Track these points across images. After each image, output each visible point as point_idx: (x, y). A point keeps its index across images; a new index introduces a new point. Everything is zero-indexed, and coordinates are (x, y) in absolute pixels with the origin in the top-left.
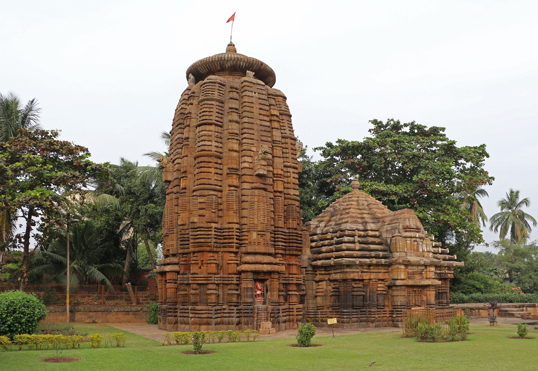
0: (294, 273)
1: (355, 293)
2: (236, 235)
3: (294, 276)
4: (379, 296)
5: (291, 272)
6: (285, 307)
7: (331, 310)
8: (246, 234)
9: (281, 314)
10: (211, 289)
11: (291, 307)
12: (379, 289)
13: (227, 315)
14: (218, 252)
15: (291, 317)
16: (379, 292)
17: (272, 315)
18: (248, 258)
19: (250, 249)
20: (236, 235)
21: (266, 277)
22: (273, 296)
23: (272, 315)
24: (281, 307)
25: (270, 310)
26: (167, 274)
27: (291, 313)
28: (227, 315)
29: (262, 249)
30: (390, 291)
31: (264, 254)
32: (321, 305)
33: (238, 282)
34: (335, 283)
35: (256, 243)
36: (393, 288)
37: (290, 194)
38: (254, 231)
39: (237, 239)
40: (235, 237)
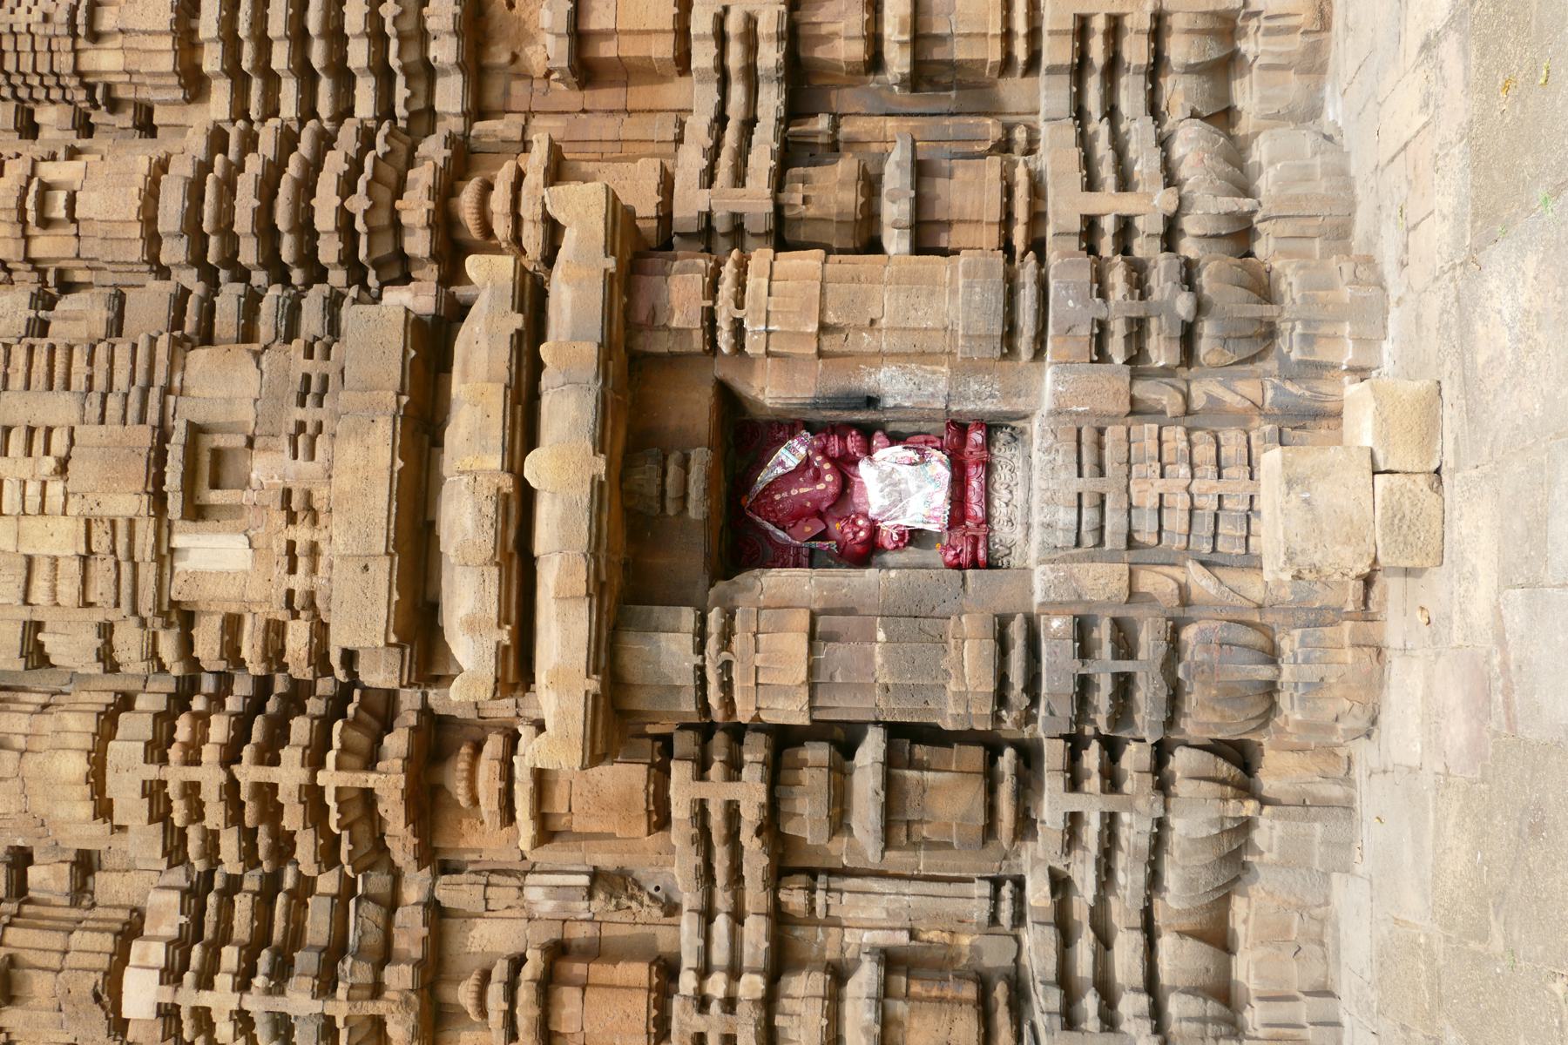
2: (230, 756)
5: (663, 48)
6: (1056, 155)
8: (207, 644)
9: (1149, 204)
11: (1057, 52)
13: (1129, 877)
14: (436, 913)
15: (1178, 50)
17: (1161, 352)
18: (471, 645)
19: (363, 620)
20: (230, 756)
21: (694, 409)
22: (911, 322)
23: (1161, 352)
24: (1066, 206)
25: (1108, 386)
26: (920, 157)
27: (1135, 51)
28: (1129, 877)
29: (363, 462)
31: (423, 425)
33: (754, 753)
35: (302, 534)
38: (165, 556)
39: (269, 755)
40: (248, 773)
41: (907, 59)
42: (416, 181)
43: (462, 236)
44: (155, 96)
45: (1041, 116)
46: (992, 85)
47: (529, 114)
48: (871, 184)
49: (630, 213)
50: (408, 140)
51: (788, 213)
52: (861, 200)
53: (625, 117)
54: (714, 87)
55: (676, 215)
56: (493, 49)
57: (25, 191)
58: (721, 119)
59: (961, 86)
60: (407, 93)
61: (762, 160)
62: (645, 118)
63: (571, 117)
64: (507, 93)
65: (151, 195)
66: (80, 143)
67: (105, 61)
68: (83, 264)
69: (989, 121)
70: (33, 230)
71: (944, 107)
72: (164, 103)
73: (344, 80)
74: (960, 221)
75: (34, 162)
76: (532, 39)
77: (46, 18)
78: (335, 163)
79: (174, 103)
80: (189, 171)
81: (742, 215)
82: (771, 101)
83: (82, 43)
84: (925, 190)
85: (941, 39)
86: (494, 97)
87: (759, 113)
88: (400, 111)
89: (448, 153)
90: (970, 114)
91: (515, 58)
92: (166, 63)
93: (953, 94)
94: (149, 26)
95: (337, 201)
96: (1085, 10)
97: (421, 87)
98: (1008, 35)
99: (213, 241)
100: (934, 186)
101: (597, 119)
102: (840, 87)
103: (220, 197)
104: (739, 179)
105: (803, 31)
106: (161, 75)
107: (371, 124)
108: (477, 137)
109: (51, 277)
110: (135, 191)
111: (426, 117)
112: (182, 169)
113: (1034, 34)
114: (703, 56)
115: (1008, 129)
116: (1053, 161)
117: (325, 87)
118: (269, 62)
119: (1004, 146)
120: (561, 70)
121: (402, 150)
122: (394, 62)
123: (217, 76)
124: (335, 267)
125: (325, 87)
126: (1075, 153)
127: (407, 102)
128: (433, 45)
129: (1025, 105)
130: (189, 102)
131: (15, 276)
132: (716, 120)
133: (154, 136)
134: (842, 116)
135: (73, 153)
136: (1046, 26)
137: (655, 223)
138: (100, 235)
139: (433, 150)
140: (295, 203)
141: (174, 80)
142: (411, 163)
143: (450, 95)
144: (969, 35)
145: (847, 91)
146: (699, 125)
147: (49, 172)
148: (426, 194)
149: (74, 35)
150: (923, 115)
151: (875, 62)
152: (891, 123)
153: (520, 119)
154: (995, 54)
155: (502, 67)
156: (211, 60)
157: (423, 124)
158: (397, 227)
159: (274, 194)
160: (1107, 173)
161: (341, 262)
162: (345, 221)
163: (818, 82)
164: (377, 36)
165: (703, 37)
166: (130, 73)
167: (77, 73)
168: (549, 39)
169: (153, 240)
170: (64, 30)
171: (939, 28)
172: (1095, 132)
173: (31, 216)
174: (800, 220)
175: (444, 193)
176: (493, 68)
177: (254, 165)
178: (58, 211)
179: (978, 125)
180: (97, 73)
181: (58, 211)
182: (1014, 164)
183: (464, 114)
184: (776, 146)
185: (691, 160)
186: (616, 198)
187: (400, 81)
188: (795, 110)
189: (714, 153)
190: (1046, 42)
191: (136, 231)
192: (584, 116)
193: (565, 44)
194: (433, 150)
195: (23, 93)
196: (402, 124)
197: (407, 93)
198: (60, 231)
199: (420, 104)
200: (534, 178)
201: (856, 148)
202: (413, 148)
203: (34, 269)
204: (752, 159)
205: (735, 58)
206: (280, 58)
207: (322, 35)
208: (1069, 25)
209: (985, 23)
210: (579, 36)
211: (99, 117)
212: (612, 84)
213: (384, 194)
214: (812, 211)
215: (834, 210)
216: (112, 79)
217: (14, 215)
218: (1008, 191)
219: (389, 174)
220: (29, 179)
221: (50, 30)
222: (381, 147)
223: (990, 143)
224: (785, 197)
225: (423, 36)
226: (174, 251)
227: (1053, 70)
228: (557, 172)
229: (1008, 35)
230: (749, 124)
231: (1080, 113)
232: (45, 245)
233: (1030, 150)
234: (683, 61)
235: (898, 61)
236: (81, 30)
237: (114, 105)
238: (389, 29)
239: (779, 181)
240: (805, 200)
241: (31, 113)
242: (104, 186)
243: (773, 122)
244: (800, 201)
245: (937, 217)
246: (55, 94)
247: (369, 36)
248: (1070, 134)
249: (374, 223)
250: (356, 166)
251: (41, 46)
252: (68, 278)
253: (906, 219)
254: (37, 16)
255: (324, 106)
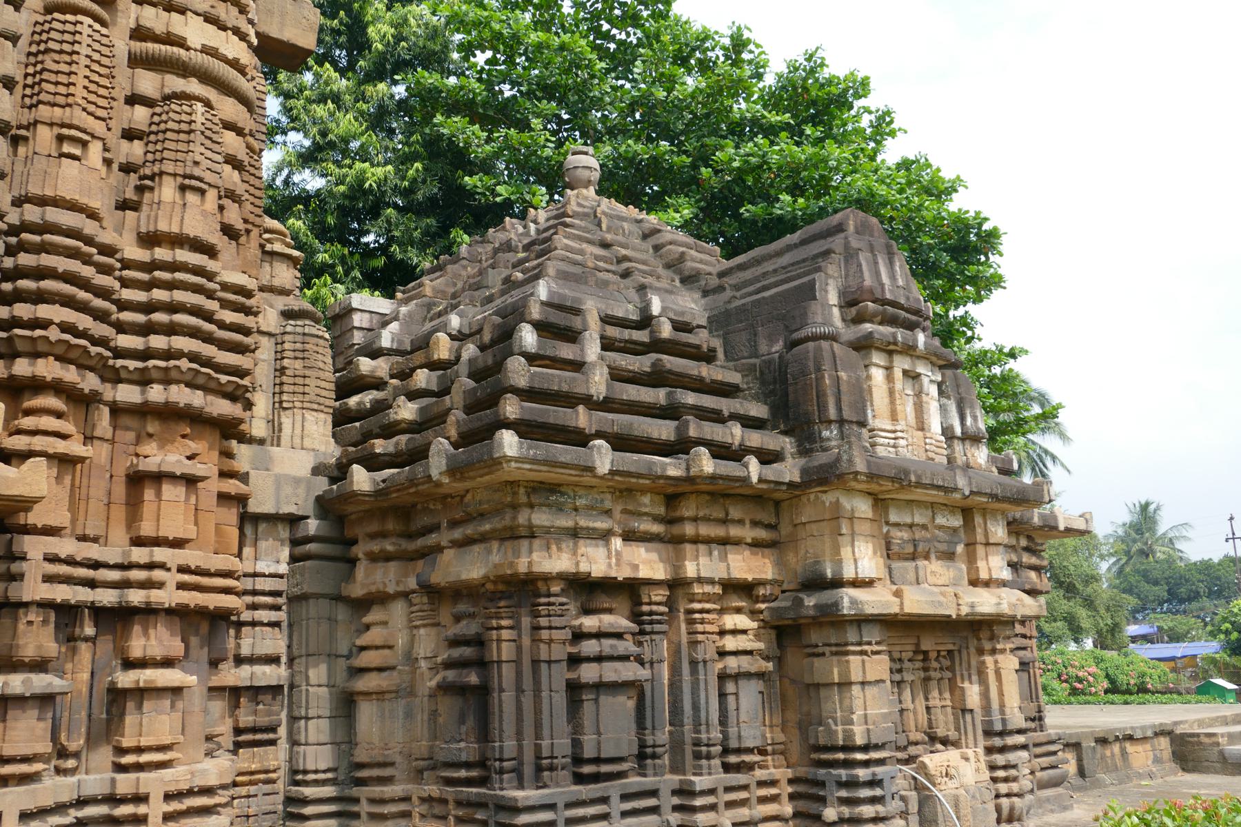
0: (169, 532)
1: (588, 673)
3: (160, 554)
4: (730, 687)
7: (433, 790)
10: (252, 660)
11: (126, 783)
12: (730, 643)
16: (732, 663)
26: (58, 698)
30: (793, 658)
32: (377, 756)
34: (462, 607)
36: (815, 637)
37: (181, 43)
41: (127, 686)
42: (68, 370)
43: (27, 395)
44: (143, 215)
45: (84, 777)
46: (108, 742)
47: (112, 441)
48: (40, 666)
49: (27, 510)
50: (99, 366)
51: (21, 611)
52: (27, 660)
53: (106, 501)
54: (119, 561)
55: (27, 537)
56: (157, 423)
57: (84, 131)
58: (96, 565)
59: (109, 721)
60: (131, 368)
61: (62, 593)
62: (103, 515)
63: (108, 467)
64: (127, 429)
65: (73, 207)
66: (115, 166)
67: (167, 191)
68: (30, 154)
69: (82, 742)
70: (56, 130)
71: (95, 711)
72: (139, 219)
73: (145, 330)
74: (5, 728)
75: (103, 139)
76: (161, 447)
77: (196, 163)
78: (84, 321)
79: (138, 226)
80: (87, 231)
81: (22, 580)
82: (107, 597)
83: (179, 180)
84: (30, 702)
85: (140, 707)
86: (125, 420)
87: (98, 590)
88: (120, 363)
89: (87, 391)
90: (89, 728)
91: (150, 436)
92: (163, 226)
93: (104, 716)
94: (186, 221)
95: (57, 321)
96: (151, 800)
97: (135, 377)
98: (139, 750)
99: (37, 238)
100: (33, 708)
101: (102, 486)
102: (114, 641)
103: (66, 248)
104: (49, 579)
105: (152, 618)
106: (156, 222)
107: (218, 279)
108: (98, 408)
109: (23, 132)
110: (77, 197)
111: (115, 377)
112: (89, 227)
113: (139, 767)
114: (139, 555)
115: (76, 755)
116: (45, 788)
117: (140, 318)
118: (159, 288)
119: (62, 753)
120: (137, 465)
121: (92, 363)
122: (151, 363)
123: (152, 255)
124: (11, 312)
125: (140, 318)
126: (49, 802)
127: (126, 368)
128: (161, 387)
129: (92, 765)
130: (138, 234)
131: (26, 110)
132: (96, 561)
133: (117, 208)
134: (94, 644)
135: (108, 162)
136: (142, 775)
137: (22, 522)
138: (49, 170)
139: (90, 382)
140: (58, 294)
141: (152, 229)
142: (80, 367)
143: (128, 394)
144: (141, 724)
145: (111, 646)
146: (93, 552)
147: (95, 148)
148: (56, 376)
149: (185, 176)
150: (91, 696)
151: (129, 664)
152: (86, 676)
153: (109, 435)
154: (126, 743)
155: (145, 427)
156: (162, 253)
157: (109, 375)
158: (35, 355)
159: (66, 282)
160: (175, 806)
161: (13, 317)
162: (45, 324)
163: (119, 627)
164: (169, 355)
165: (151, 555)
166: (159, 203)
167: (161, 173)
168: (158, 459)
169: (42, 202)
170: (188, 171)
171: (147, 705)
172: (68, 815)
173: (65, 131)
174: (16, 620)
175: (57, 387)
176: (145, 421)
177: (87, 271)
178: (67, 148)
179: (80, 734)
180: (160, 185)
181: (67, 148)
182: (47, 761)
183: (115, 402)
184: (73, 602)
185: (66, 546)
186: (36, 502)
187: (140, 365)
188: (100, 613)
189: (71, 561)
190: (132, 776)
191: (49, 192)
192: (108, 476)
193: (155, 469)
194: (90, 382)
195: (152, 138)
196: (111, 362)
197: (131, 368)
198: (54, 146)
199: (123, 375)
200: (60, 446)
201: (69, 654)
202: (92, 369)
203: (30, 124)
204: (64, 586)
205: (137, 575)
206: (159, 295)
207: (171, 321)
208: (142, 790)
209: (148, 735)
210: (159, 478)
211: (133, 179)
212: (128, 495)
213: (60, 350)
214: (21, 626)
215: (21, 642)
216: (156, 193)
217: (68, 122)
218: (25, 760)
219: (73, 355)
220: (93, 136)
221: (189, 163)
222: (94, 350)
223: (66, 744)
224: (34, 608)
225: (167, 382)
226: (32, 213)
227: (113, 781)
228: (65, 462)
229: (139, 750)
230: (92, 584)
231: (81, 802)
232: (45, 136)
233: (58, 771)
234: (138, 542)
235: (126, 679)
236: (187, 182)
237: (140, 189)
238: (172, 363)
239: (45, 605)
240: (30, 623)
241: (141, 139)
242: (83, 179)
243: (91, 599)
244: (29, 618)
245: (10, 712)
246: (150, 157)
247: (169, 350)
248: (65, 798)
249: (39, 342)
250: (83, 334)
251: (180, 156)
252: (21, 142)
253: (9, 691)
254: (198, 158)
255: (127, 316)
